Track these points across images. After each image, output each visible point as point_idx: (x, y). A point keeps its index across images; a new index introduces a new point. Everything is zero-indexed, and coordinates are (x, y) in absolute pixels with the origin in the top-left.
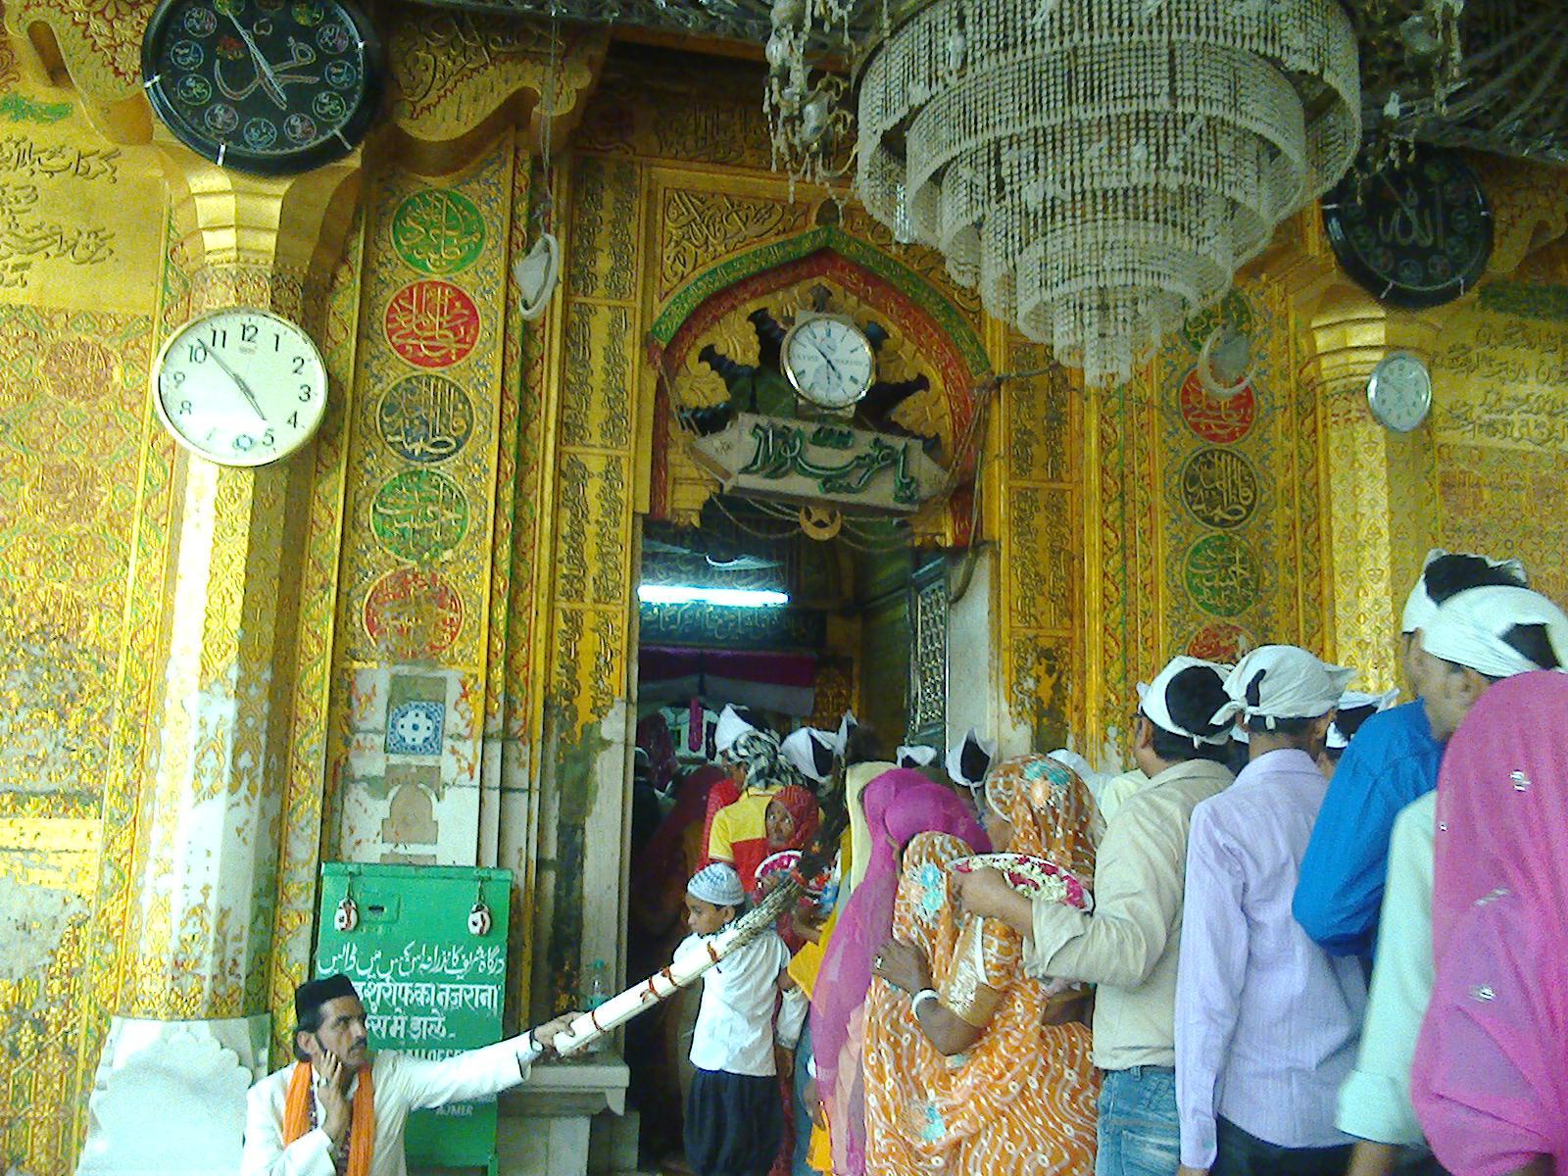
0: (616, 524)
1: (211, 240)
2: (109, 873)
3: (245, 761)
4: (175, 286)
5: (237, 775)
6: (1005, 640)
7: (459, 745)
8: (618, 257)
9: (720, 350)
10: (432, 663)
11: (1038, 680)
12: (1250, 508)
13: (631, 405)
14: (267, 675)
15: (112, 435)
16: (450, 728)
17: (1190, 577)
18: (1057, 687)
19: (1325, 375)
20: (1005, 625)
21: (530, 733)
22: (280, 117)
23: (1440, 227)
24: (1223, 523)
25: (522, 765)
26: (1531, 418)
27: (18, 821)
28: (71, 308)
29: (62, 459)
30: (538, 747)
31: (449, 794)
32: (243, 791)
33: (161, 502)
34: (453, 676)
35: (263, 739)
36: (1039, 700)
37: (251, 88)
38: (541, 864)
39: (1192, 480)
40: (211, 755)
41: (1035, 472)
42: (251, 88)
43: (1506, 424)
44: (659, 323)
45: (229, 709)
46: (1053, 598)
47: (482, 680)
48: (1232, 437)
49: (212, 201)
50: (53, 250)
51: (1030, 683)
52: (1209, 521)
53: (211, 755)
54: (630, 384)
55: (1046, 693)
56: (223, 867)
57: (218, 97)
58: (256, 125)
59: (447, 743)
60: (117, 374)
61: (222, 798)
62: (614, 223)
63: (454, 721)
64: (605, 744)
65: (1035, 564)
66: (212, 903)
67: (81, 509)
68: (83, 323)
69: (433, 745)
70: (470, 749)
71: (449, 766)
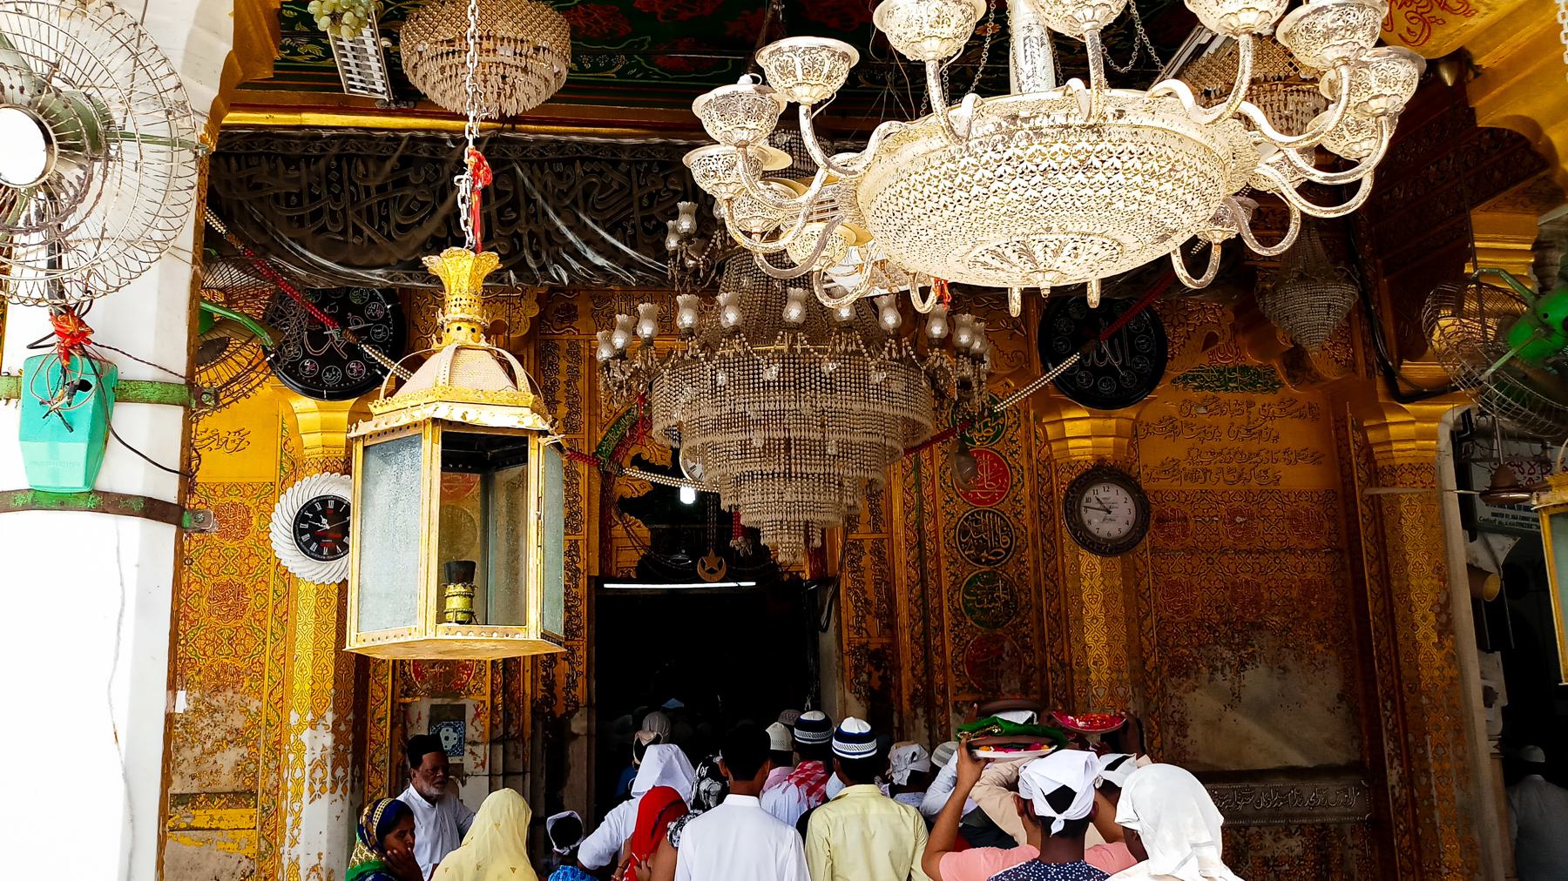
0: (577, 586)
1: (308, 440)
2: (263, 843)
3: (340, 772)
4: (288, 467)
5: (335, 783)
6: (845, 647)
7: (475, 749)
8: (570, 406)
9: (646, 457)
10: (457, 696)
11: (870, 674)
12: (1008, 550)
13: (583, 504)
14: (351, 717)
15: (253, 561)
16: (468, 736)
17: (965, 602)
18: (883, 678)
19: (1055, 455)
20: (845, 636)
21: (522, 735)
22: (342, 364)
23: (1127, 351)
24: (988, 562)
25: (518, 757)
26: (1225, 465)
27: (209, 812)
28: (227, 481)
29: (224, 578)
30: (528, 744)
31: (469, 780)
32: (339, 791)
33: (282, 609)
34: (469, 703)
35: (349, 757)
36: (871, 689)
37: (326, 347)
38: (788, 476)
39: (965, 533)
40: (319, 770)
41: (860, 528)
42: (326, 347)
43: (1206, 471)
44: (601, 445)
45: (328, 740)
46: (878, 616)
47: (488, 704)
48: (993, 500)
49: (308, 416)
50: (213, 446)
51: (864, 677)
52: (978, 561)
53: (319, 770)
54: (583, 490)
55: (876, 684)
56: (329, 841)
57: (306, 355)
58: (330, 370)
59: (468, 747)
60: (254, 521)
61: (326, 797)
62: (568, 383)
63: (471, 733)
64: (576, 736)
65: (864, 592)
66: (323, 863)
67: (237, 610)
68: (234, 491)
69: (459, 749)
70: (481, 750)
71: (469, 763)
